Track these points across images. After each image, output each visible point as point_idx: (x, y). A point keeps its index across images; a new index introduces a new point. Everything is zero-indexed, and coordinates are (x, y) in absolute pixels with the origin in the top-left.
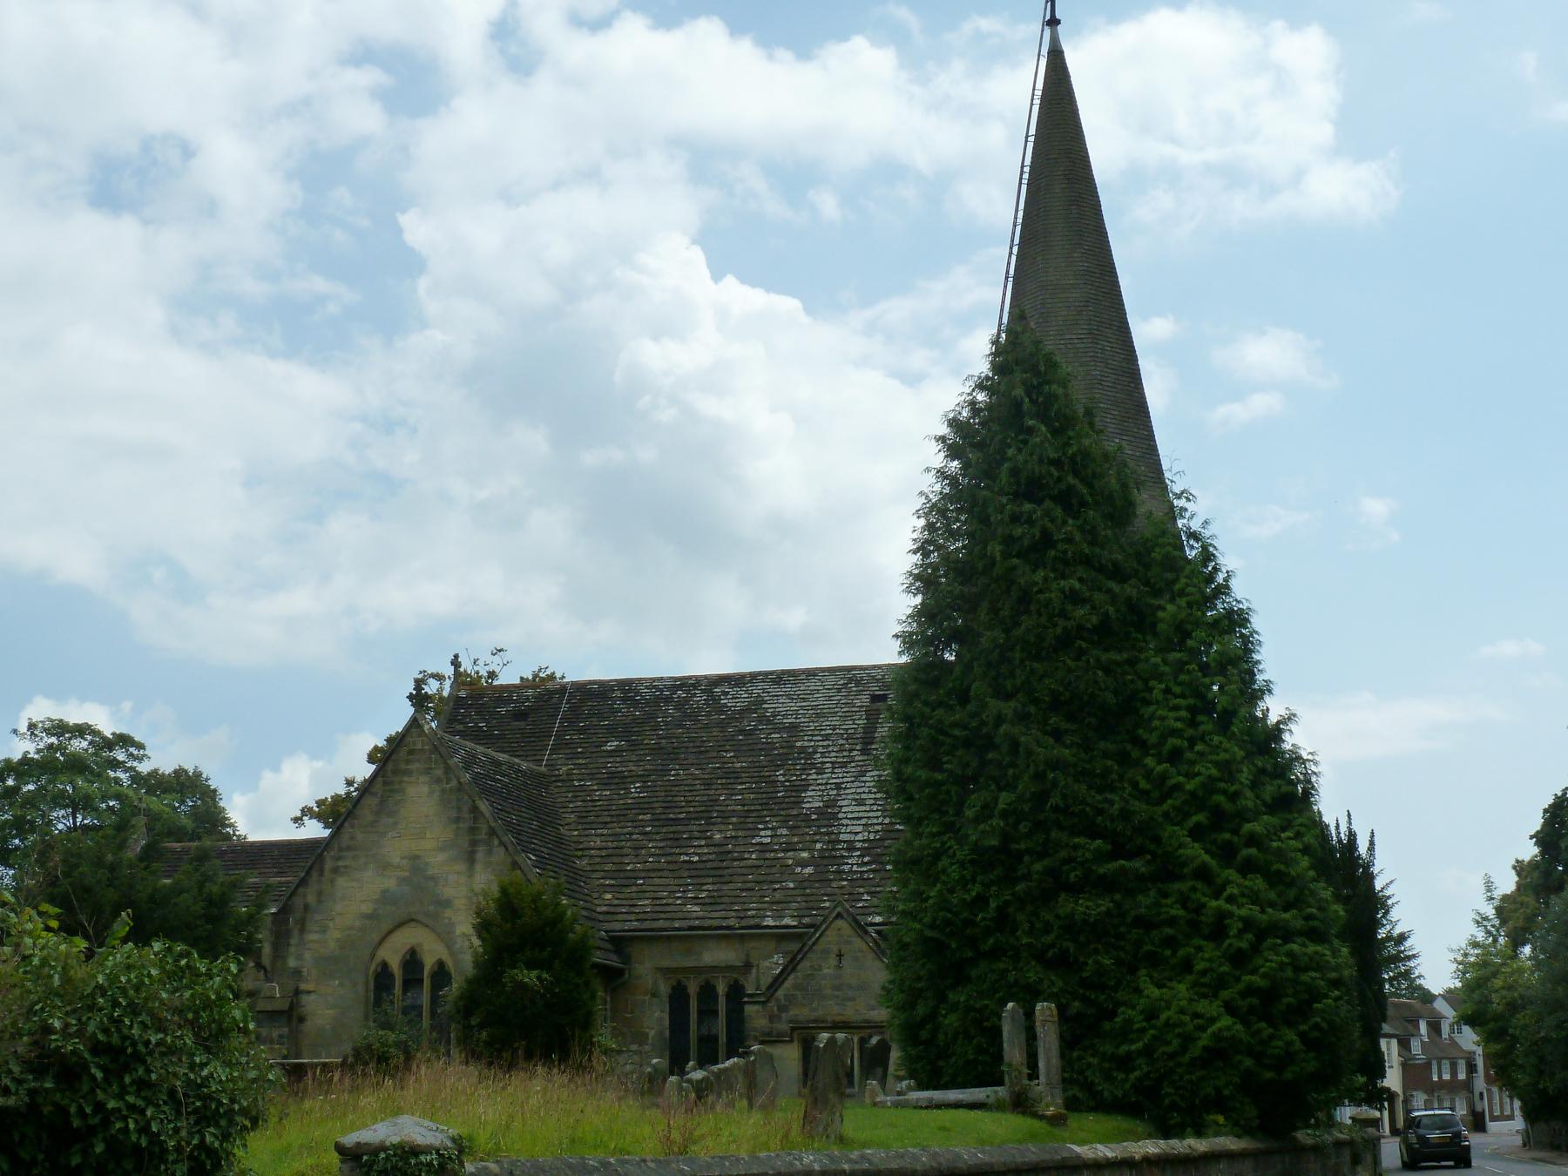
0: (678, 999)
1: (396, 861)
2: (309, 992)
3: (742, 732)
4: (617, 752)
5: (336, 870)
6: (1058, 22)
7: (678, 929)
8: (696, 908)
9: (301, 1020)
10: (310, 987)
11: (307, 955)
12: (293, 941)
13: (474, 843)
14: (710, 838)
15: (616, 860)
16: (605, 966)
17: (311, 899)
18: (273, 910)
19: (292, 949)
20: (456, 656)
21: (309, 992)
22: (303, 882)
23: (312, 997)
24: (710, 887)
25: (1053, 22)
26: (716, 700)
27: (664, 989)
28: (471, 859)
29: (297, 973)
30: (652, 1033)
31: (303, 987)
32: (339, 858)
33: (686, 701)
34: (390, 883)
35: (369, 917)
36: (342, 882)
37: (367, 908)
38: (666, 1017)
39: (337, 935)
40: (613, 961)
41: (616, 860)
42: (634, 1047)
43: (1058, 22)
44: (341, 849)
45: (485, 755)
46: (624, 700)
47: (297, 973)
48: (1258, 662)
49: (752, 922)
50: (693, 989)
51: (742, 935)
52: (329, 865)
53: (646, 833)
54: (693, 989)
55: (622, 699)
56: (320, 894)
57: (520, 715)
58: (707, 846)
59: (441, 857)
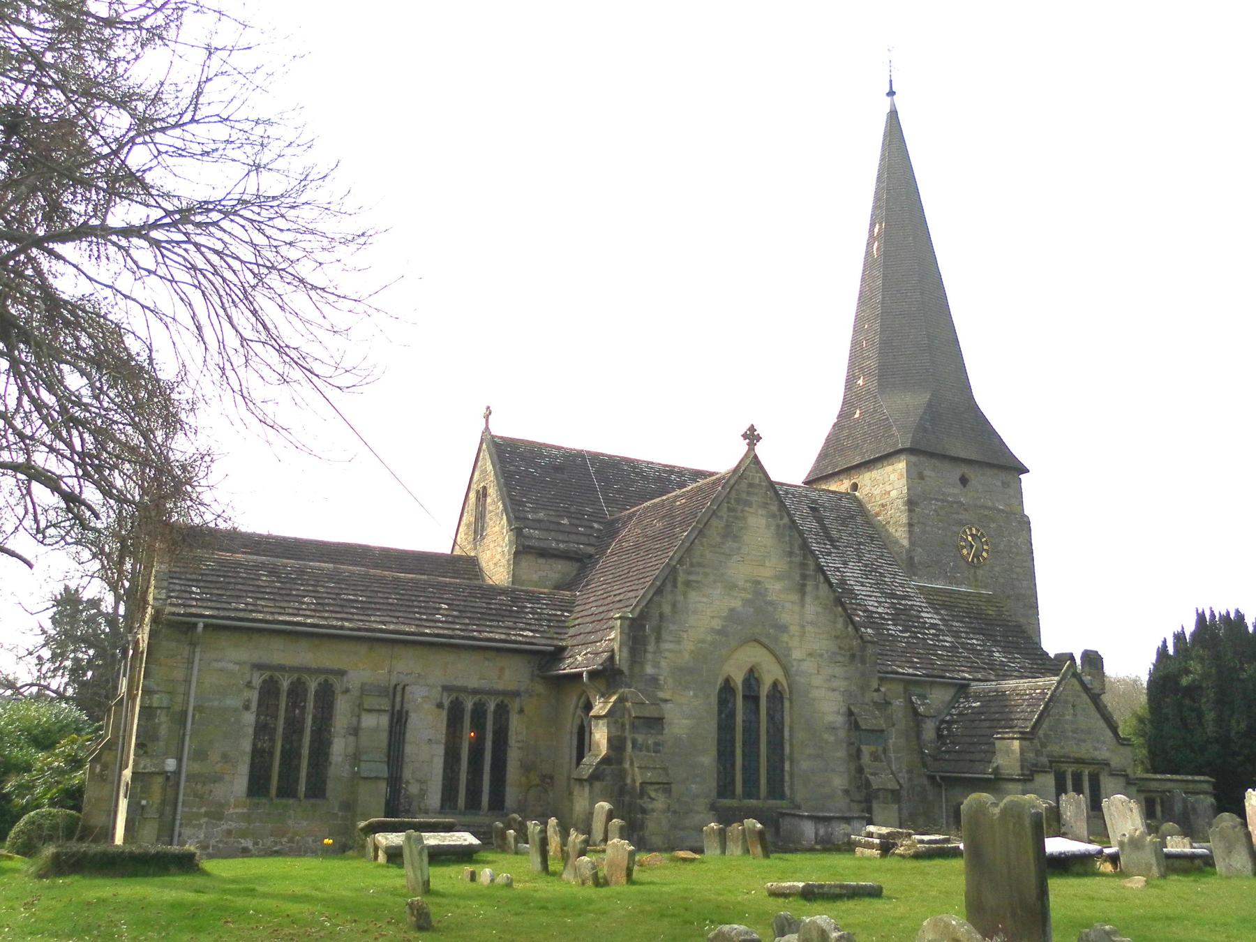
2: (666, 701)
5: (688, 584)
10: (667, 696)
12: (651, 648)
13: (804, 577)
19: (649, 656)
23: (669, 705)
29: (654, 680)
36: (693, 596)
37: (717, 624)
44: (692, 565)
47: (654, 680)
59: (778, 586)
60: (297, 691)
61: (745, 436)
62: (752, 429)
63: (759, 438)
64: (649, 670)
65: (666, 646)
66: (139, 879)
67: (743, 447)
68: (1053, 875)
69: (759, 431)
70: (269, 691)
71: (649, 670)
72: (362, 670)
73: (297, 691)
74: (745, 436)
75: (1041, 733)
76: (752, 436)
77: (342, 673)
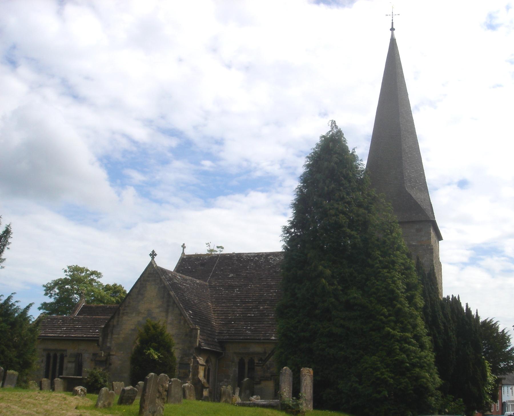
0: (241, 364)
1: (143, 311)
2: (113, 355)
3: (275, 272)
4: (232, 277)
5: (123, 314)
6: (394, 29)
7: (242, 339)
8: (249, 332)
9: (110, 364)
10: (114, 353)
11: (113, 342)
12: (109, 337)
13: (168, 306)
14: (259, 308)
15: (226, 315)
16: (214, 351)
17: (115, 323)
18: (103, 326)
19: (109, 340)
20: (184, 244)
21: (113, 355)
22: (113, 317)
23: (114, 357)
24: (256, 325)
25: (392, 29)
26: (268, 261)
27: (237, 360)
28: (167, 312)
29: (109, 348)
30: (232, 375)
31: (111, 353)
32: (124, 310)
33: (258, 261)
34: (140, 319)
35: (132, 330)
36: (125, 318)
37: (132, 327)
38: (237, 369)
39: (123, 336)
40: (219, 350)
41: (226, 315)
42: (225, 380)
43: (394, 29)
44: (125, 307)
45: (181, 277)
46: (237, 260)
47: (109, 348)
48: (9, 243)
49: (267, 338)
50: (246, 361)
51: (263, 342)
52: (121, 312)
53: (237, 306)
54: (246, 361)
55: (237, 260)
56: (118, 321)
57: (202, 265)
58: (257, 311)
59: (157, 310)
60: (55, 356)
61: (150, 255)
62: (153, 252)
63: (156, 255)
64: (108, 345)
65: (114, 336)
66: (439, 286)
67: (150, 259)
68: (170, 272)
69: (156, 252)
70: (48, 357)
71: (108, 345)
72: (71, 350)
73: (55, 356)
74: (150, 255)
75: (268, 363)
76: (153, 255)
77: (66, 350)
